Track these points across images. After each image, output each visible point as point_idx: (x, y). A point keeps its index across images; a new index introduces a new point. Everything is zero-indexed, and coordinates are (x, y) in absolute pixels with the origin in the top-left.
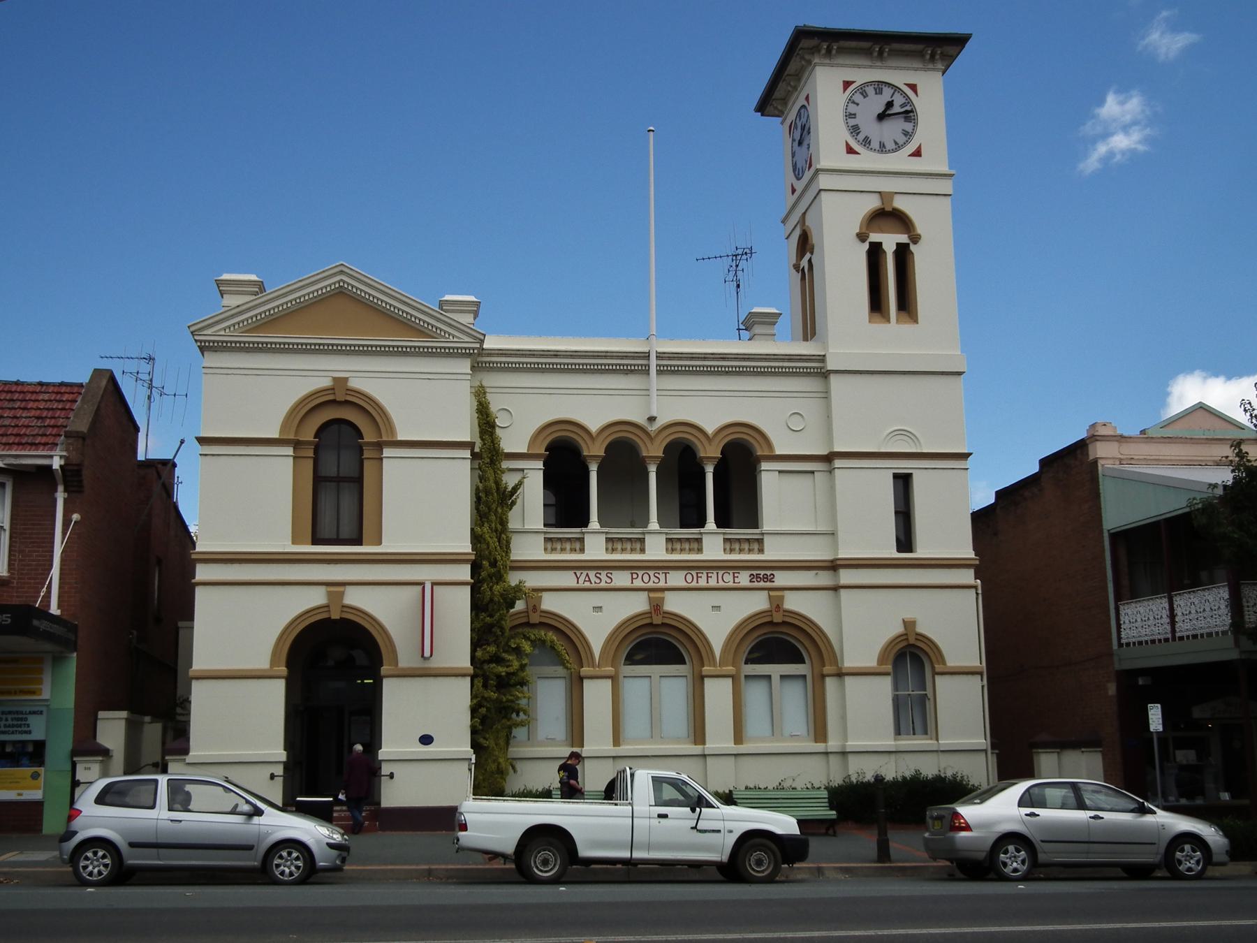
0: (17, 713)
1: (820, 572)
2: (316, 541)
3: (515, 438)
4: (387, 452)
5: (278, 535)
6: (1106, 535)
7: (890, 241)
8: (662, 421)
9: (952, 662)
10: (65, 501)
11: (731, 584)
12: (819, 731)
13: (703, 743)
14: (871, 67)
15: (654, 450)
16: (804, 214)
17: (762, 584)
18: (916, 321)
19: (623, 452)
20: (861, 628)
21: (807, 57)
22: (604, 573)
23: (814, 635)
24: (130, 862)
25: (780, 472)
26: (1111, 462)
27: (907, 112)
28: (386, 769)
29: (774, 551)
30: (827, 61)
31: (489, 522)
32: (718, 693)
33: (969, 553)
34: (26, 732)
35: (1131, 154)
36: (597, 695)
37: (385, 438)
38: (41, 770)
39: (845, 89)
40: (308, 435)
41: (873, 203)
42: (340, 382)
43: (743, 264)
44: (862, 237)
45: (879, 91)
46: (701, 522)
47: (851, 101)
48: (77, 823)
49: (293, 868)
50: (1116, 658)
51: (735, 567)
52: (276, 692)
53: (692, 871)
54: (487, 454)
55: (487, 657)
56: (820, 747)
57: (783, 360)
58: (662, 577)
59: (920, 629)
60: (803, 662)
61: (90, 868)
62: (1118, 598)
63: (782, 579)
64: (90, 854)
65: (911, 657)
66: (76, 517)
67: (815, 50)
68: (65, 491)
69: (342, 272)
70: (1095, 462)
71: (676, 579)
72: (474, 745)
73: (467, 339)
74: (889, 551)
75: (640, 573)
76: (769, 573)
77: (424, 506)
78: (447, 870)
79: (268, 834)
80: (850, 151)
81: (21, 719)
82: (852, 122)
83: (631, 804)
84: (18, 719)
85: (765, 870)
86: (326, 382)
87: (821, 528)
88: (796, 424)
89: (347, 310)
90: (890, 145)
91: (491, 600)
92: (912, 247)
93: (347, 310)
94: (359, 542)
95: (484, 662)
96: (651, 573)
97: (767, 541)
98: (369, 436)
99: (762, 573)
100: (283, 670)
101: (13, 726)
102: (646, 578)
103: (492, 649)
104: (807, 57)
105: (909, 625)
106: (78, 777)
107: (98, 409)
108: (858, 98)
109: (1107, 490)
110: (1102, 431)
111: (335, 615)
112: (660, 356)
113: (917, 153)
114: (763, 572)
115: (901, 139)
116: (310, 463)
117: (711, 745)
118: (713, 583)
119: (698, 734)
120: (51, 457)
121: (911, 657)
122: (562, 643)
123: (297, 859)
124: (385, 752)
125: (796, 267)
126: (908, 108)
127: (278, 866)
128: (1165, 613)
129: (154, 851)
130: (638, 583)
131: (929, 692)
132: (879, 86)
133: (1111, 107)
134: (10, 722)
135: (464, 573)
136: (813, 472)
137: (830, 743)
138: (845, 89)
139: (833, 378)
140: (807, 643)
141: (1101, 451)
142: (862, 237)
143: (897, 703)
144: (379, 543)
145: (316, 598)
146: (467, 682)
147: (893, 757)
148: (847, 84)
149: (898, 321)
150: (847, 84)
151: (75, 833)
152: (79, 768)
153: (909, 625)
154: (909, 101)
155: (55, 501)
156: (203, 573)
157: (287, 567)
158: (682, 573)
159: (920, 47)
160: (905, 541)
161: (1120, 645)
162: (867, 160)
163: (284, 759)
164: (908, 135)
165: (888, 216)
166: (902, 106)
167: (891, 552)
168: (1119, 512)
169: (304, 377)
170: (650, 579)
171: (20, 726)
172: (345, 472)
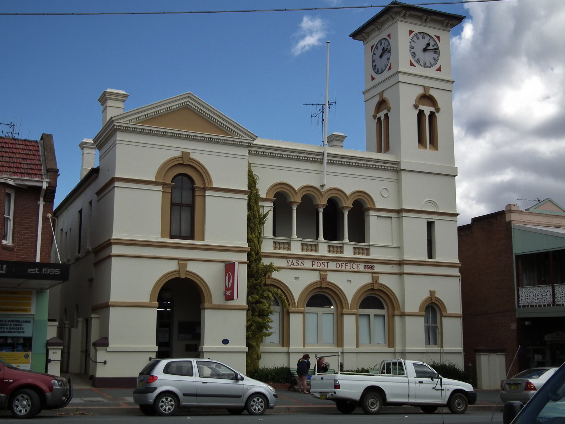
0: (17, 321)
1: (395, 266)
2: (172, 237)
3: (263, 190)
6: (514, 256)
7: (381, 115)
8: (326, 188)
11: (356, 270)
12: (391, 342)
13: (288, 346)
14: (421, 25)
16: (383, 91)
17: (369, 270)
18: (437, 149)
20: (412, 293)
21: (393, 16)
22: (300, 261)
23: (389, 294)
24: (184, 404)
25: (378, 216)
26: (516, 222)
27: (435, 49)
29: (374, 255)
30: (403, 20)
31: (255, 232)
32: (349, 322)
33: (457, 261)
34: (21, 332)
35: (313, 48)
36: (295, 321)
37: (207, 186)
38: (30, 353)
39: (410, 34)
40: (169, 181)
41: (420, 91)
44: (416, 107)
45: (424, 38)
47: (412, 40)
48: (155, 384)
49: (259, 407)
50: (517, 313)
51: (358, 261)
52: (151, 315)
53: (429, 409)
54: (253, 199)
55: (254, 300)
56: (391, 350)
57: (381, 162)
58: (326, 264)
59: (437, 295)
60: (383, 308)
61: (164, 407)
62: (518, 285)
64: (164, 400)
67: (398, 13)
68: (44, 200)
69: (189, 97)
70: (510, 222)
71: (332, 266)
72: (248, 345)
73: (248, 138)
74: (424, 258)
75: (316, 262)
76: (372, 265)
77: (224, 222)
78: (296, 408)
79: (248, 390)
80: (412, 64)
81: (19, 325)
82: (413, 51)
83: (406, 377)
84: (17, 325)
85: (375, 409)
86: (179, 154)
87: (395, 245)
88: (385, 194)
89: (191, 117)
90: (428, 64)
91: (257, 272)
92: (436, 114)
93: (191, 117)
94: (192, 238)
95: (253, 303)
96: (321, 262)
97: (372, 249)
98: (198, 184)
99: (369, 265)
101: (14, 328)
102: (319, 265)
103: (257, 297)
104: (393, 16)
105: (432, 293)
106: (50, 357)
108: (415, 39)
109: (515, 236)
110: (513, 208)
111: (183, 276)
112: (329, 155)
114: (370, 264)
115: (433, 62)
116: (169, 196)
117: (346, 348)
118: (348, 268)
120: (42, 182)
121: (433, 308)
122: (282, 296)
123: (261, 402)
125: (374, 117)
126: (436, 47)
127: (253, 406)
129: (195, 398)
130: (315, 267)
131: (438, 325)
132: (424, 35)
133: (307, 23)
134: (13, 326)
136: (391, 218)
137: (397, 348)
138: (410, 34)
139: (403, 174)
140: (334, 296)
141: (514, 218)
143: (427, 329)
144: (203, 239)
145: (173, 266)
146: (245, 313)
147: (425, 355)
148: (411, 32)
150: (411, 32)
151: (156, 388)
152: (51, 353)
153: (432, 293)
154: (436, 44)
155: (38, 206)
160: (430, 254)
161: (519, 306)
162: (418, 70)
163: (157, 350)
164: (436, 60)
165: (427, 98)
166: (433, 46)
167: (425, 258)
168: (520, 246)
169: (171, 149)
171: (18, 329)
172: (184, 202)
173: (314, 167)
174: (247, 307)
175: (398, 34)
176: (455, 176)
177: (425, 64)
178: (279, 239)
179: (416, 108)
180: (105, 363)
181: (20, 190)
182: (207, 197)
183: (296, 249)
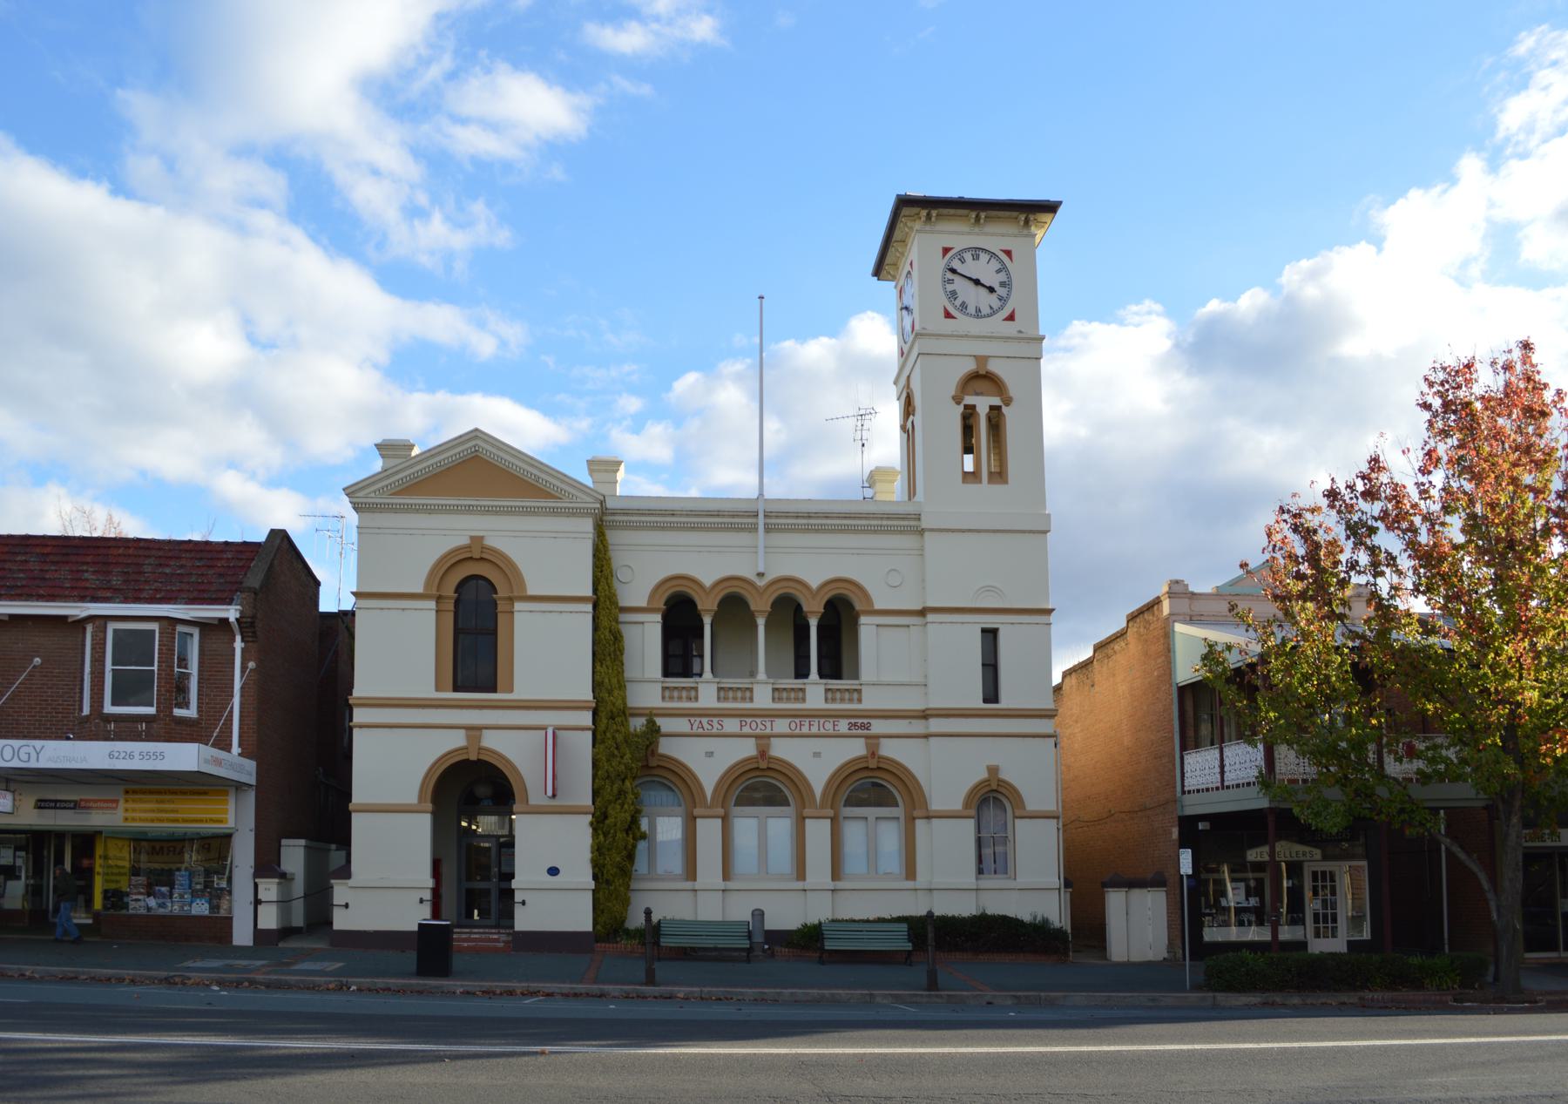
2: (456, 689)
4: (518, 606)
7: (983, 404)
9: (1031, 805)
10: (243, 651)
15: (760, 606)
19: (734, 605)
22: (715, 720)
28: (518, 897)
29: (871, 701)
41: (970, 366)
42: (477, 540)
43: (867, 424)
44: (957, 400)
46: (806, 675)
52: (422, 824)
59: (1003, 775)
62: (1184, 748)
63: (878, 727)
65: (992, 798)
66: (251, 665)
71: (781, 726)
74: (977, 702)
77: (548, 653)
80: (948, 315)
86: (465, 541)
92: (1005, 410)
94: (494, 690)
97: (866, 692)
98: (502, 592)
100: (429, 806)
105: (993, 770)
106: (260, 896)
107: (271, 565)
111: (473, 757)
113: (1011, 318)
114: (860, 721)
116: (451, 616)
118: (814, 730)
119: (801, 872)
121: (992, 798)
124: (515, 884)
128: (1217, 763)
130: (746, 730)
135: (586, 718)
145: (457, 740)
148: (946, 250)
150: (946, 250)
153: (993, 770)
156: (359, 716)
157: (477, 712)
158: (736, 721)
159: (1015, 214)
161: (1183, 792)
173: (743, 539)
174: (592, 809)
175: (74, 538)
176: (1045, 532)
177: (978, 310)
178: (729, 682)
179: (958, 403)
180: (347, 906)
181: (204, 626)
182: (516, 615)
183: (763, 698)
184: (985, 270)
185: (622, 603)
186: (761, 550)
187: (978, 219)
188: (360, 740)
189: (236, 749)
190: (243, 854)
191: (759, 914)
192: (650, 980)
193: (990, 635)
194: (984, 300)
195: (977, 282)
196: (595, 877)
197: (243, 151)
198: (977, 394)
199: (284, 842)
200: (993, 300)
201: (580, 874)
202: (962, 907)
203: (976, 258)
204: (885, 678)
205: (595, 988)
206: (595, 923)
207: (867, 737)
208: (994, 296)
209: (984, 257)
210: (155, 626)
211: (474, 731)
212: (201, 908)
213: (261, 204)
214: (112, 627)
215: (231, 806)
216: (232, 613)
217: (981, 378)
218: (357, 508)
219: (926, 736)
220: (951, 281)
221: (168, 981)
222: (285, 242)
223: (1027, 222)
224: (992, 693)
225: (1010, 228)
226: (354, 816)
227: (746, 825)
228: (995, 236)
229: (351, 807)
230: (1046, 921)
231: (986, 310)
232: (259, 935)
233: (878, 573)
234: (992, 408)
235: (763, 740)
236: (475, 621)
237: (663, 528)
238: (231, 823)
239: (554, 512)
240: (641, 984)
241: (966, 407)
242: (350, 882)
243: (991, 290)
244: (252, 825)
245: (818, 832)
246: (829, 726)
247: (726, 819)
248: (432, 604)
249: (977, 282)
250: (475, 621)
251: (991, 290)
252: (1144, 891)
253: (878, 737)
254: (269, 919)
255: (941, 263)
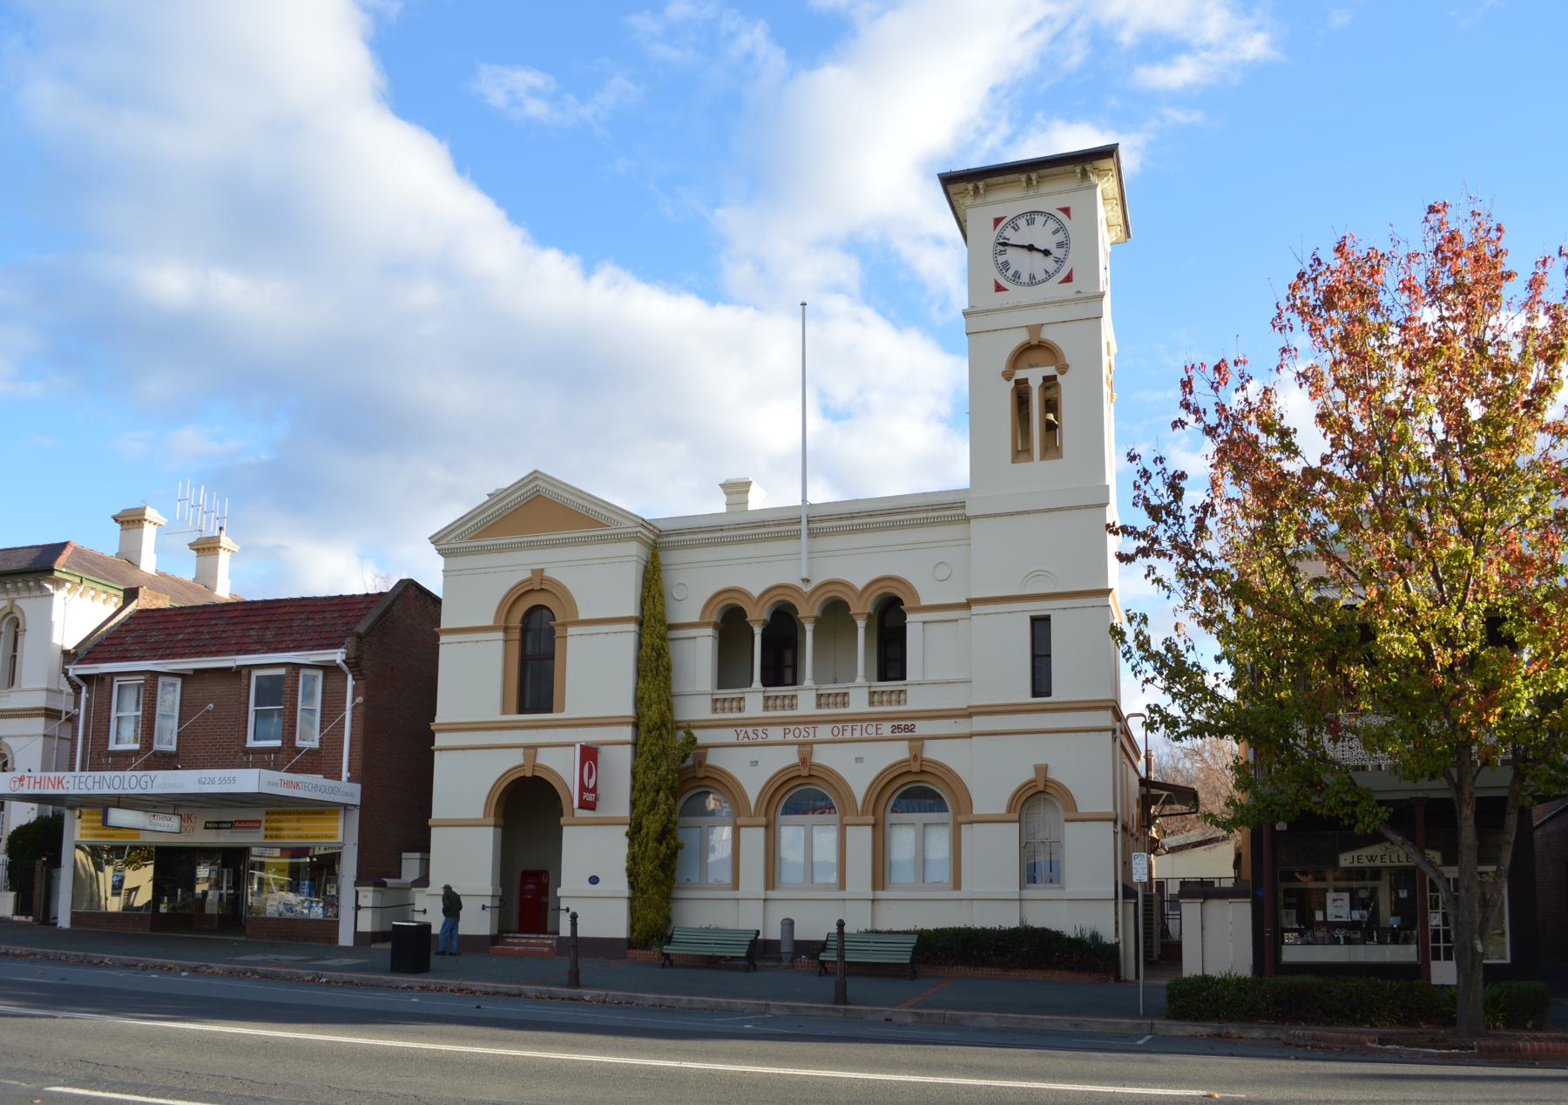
2: (522, 709)
5: (491, 710)
7: (1035, 377)
9: (1084, 807)
22: (760, 729)
27: (1004, 244)
29: (917, 700)
40: (516, 621)
41: (1022, 337)
44: (1007, 376)
59: (1052, 775)
63: (923, 728)
71: (824, 732)
74: (1024, 695)
77: (598, 675)
80: (999, 288)
86: (528, 575)
92: (1060, 379)
94: (550, 710)
100: (492, 820)
105: (1042, 770)
111: (529, 774)
113: (1068, 279)
114: (904, 723)
118: (857, 735)
121: (1037, 796)
130: (790, 737)
135: (626, 733)
142: (1007, 376)
144: (1049, 695)
145: (515, 759)
149: (1043, 458)
150: (997, 221)
153: (1042, 770)
156: (440, 740)
157: (533, 732)
159: (1070, 168)
170: (804, 733)
177: (1032, 277)
178: (774, 691)
179: (1008, 379)
183: (859, 702)
184: (1041, 235)
185: (671, 620)
186: (804, 556)
187: (1029, 180)
188: (440, 761)
189: (345, 774)
190: (348, 868)
191: (789, 925)
192: (574, 981)
193: (1040, 625)
194: (1038, 264)
195: (1031, 248)
196: (632, 886)
197: (822, 244)
198: (1031, 366)
199: (404, 855)
200: (1049, 263)
201: (617, 883)
202: (1006, 919)
203: (1031, 222)
204: (930, 677)
205: (514, 988)
206: (632, 928)
207: (910, 740)
208: (1050, 259)
209: (1040, 220)
210: (282, 671)
211: (530, 749)
212: (318, 912)
213: (836, 289)
214: (255, 673)
215: (341, 825)
216: (338, 656)
217: (1035, 349)
218: (442, 552)
219: (971, 736)
220: (1002, 253)
221: (195, 970)
222: (859, 320)
223: (1084, 174)
224: (1041, 683)
225: (1071, 184)
226: (433, 830)
227: (791, 834)
228: (1050, 196)
229: (430, 822)
230: (1095, 936)
231: (1040, 276)
232: (358, 935)
233: (924, 571)
234: (1046, 379)
235: (806, 747)
236: (536, 644)
237: (715, 544)
238: (340, 839)
239: (603, 540)
240: (562, 986)
241: (1017, 382)
242: (428, 890)
243: (1047, 253)
244: (356, 840)
245: (860, 838)
246: (872, 730)
247: (771, 829)
248: (500, 635)
249: (1031, 248)
250: (536, 644)
251: (1047, 253)
252: (1225, 902)
253: (922, 739)
254: (366, 924)
255: (992, 236)
